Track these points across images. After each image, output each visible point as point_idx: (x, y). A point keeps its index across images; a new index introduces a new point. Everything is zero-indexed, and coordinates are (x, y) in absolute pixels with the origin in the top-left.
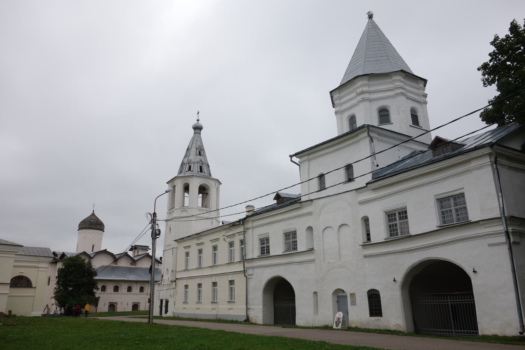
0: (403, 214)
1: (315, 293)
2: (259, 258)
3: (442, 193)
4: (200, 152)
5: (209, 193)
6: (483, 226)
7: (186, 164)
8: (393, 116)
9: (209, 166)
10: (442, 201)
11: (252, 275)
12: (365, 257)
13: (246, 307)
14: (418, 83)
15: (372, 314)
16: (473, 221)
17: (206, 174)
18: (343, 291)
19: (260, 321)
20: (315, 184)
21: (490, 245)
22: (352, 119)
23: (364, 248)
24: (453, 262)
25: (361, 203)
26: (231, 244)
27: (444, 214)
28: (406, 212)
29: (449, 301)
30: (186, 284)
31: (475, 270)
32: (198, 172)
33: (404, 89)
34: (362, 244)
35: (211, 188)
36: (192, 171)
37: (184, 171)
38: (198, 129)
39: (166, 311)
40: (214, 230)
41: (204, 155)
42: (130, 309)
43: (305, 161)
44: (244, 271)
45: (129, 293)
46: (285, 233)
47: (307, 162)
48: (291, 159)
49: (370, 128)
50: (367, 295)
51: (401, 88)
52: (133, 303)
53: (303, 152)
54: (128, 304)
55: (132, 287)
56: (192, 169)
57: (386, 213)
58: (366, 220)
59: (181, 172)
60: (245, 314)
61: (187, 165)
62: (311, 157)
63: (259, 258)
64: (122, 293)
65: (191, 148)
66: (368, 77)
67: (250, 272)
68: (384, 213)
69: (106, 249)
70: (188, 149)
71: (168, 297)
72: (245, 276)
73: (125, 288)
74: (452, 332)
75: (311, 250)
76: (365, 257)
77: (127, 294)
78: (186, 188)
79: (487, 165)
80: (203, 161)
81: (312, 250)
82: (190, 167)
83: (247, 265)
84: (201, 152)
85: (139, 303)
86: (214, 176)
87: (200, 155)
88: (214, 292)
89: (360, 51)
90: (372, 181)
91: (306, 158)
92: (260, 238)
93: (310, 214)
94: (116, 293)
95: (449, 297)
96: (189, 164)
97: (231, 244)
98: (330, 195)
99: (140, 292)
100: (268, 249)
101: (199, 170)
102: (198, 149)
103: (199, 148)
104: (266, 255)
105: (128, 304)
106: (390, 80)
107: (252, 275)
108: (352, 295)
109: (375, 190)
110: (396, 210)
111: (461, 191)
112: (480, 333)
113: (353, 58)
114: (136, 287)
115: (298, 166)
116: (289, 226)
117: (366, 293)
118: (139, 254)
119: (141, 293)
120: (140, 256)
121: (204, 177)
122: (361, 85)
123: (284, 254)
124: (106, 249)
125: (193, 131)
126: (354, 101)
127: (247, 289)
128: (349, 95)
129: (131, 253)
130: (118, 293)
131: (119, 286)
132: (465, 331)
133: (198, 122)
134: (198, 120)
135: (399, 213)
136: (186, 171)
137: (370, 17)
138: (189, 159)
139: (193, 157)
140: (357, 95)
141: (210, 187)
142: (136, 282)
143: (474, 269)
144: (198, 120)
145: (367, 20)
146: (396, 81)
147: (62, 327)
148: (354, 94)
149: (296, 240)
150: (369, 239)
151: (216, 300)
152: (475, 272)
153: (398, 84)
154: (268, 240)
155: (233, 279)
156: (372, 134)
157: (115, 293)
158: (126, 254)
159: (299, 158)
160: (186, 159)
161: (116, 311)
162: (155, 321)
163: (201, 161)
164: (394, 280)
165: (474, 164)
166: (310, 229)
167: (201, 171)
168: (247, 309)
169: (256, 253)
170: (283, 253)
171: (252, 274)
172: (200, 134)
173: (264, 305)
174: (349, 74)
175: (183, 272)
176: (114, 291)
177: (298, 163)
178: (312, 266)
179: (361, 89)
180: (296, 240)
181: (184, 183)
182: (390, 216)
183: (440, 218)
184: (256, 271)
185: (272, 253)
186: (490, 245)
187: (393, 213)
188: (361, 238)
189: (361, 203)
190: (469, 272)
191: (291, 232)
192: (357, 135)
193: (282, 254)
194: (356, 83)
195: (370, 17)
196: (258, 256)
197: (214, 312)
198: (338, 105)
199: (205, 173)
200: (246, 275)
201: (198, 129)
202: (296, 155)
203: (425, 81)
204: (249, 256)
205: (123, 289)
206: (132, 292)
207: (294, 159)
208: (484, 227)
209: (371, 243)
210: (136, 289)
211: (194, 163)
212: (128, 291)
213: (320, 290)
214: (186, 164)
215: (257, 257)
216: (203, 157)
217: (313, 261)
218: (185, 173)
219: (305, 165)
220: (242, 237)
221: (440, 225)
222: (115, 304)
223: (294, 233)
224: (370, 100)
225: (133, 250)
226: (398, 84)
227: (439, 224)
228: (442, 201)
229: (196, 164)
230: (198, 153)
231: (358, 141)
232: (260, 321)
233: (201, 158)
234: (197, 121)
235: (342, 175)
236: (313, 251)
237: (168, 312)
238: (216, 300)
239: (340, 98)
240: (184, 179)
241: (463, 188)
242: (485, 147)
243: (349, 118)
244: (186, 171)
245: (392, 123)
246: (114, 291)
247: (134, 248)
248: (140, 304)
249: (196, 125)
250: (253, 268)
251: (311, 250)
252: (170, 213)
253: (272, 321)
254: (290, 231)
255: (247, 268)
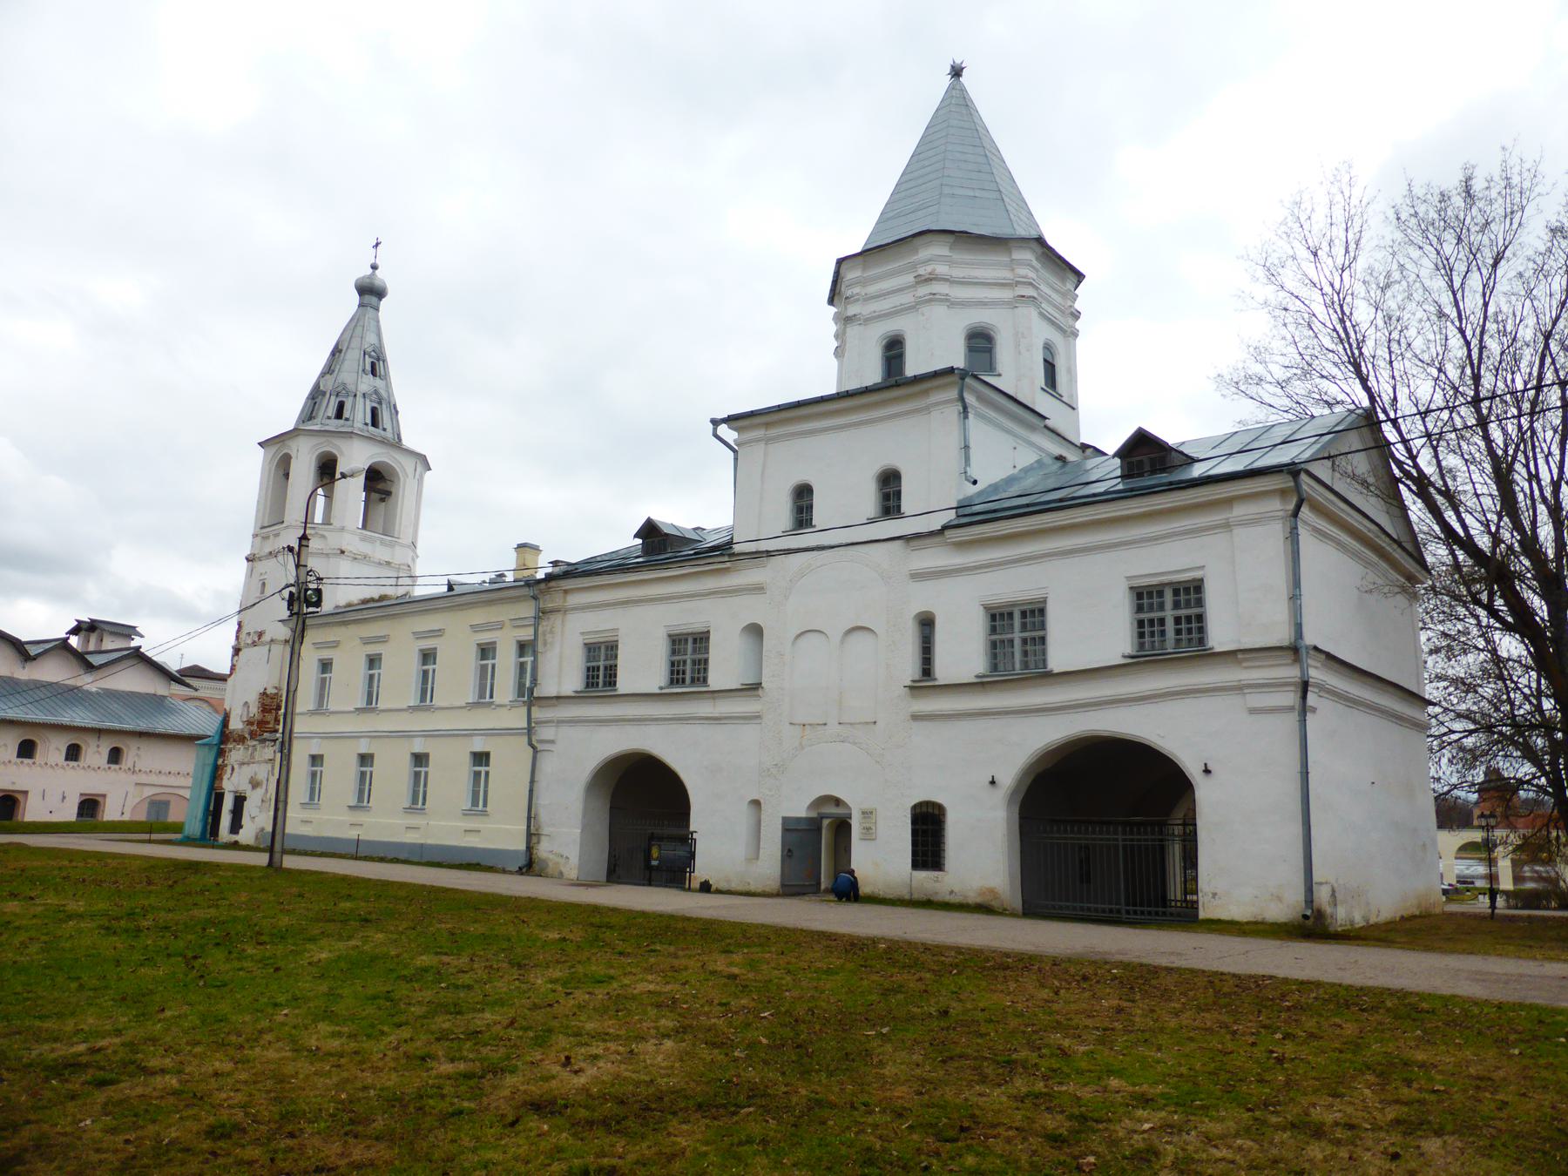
0: (1035, 614)
1: (756, 804)
2: (577, 698)
3: (1147, 572)
4: (373, 365)
5: (393, 490)
6: (1245, 664)
7: (328, 395)
8: (1004, 354)
9: (397, 412)
10: (1145, 596)
11: (552, 742)
12: (916, 717)
13: (525, 827)
14: (1063, 280)
15: (917, 864)
16: (1218, 649)
17: (389, 435)
18: (838, 802)
19: (571, 871)
20: (781, 513)
21: (1253, 711)
22: (894, 350)
23: (913, 696)
24: (1152, 745)
25: (917, 576)
26: (486, 651)
27: (1146, 629)
28: (1042, 612)
29: (1120, 837)
30: (314, 752)
31: (1209, 768)
32: (366, 424)
33: (1037, 288)
34: (909, 683)
35: (402, 479)
36: (347, 419)
37: (321, 413)
38: (370, 292)
39: (236, 826)
40: (427, 603)
41: (385, 378)
42: (69, 813)
43: (758, 440)
44: (530, 731)
45: (72, 764)
46: (670, 636)
47: (762, 445)
48: (715, 430)
49: (968, 380)
50: (909, 816)
51: (1031, 284)
52: (81, 795)
53: (752, 414)
54: (64, 798)
55: (125, 750)
56: (346, 414)
57: (987, 608)
58: (926, 624)
59: (309, 413)
60: (522, 847)
61: (333, 398)
62: (773, 432)
63: (577, 698)
64: (46, 764)
65: (348, 348)
66: (951, 238)
67: (545, 733)
68: (982, 608)
69: (140, 647)
70: (337, 351)
71: (244, 787)
72: (531, 745)
73: (58, 749)
74: (1119, 911)
75: (754, 688)
76: (916, 717)
77: (63, 767)
78: (327, 470)
79: (1274, 518)
80: (384, 394)
81: (756, 689)
82: (341, 406)
83: (537, 713)
84: (376, 365)
85: (104, 796)
86: (408, 441)
87: (374, 372)
88: (418, 782)
89: (926, 163)
90: (956, 522)
91: (759, 433)
92: (586, 641)
93: (758, 589)
94: (26, 761)
95: (1120, 829)
96: (337, 395)
97: (486, 651)
98: (833, 543)
99: (110, 762)
100: (610, 675)
101: (369, 420)
102: (370, 356)
103: (373, 353)
104: (601, 690)
105: (64, 798)
106: (1004, 258)
107: (552, 742)
108: (867, 814)
109: (961, 545)
110: (1014, 604)
111: (1197, 574)
112: (1202, 915)
113: (904, 179)
114: (98, 746)
115: (732, 453)
116: (688, 617)
117: (909, 811)
118: (104, 648)
119: (113, 766)
120: (107, 655)
121: (384, 442)
122: (934, 256)
123: (664, 691)
124: (140, 647)
125: (356, 298)
126: (906, 298)
127: (532, 782)
128: (892, 279)
129: (74, 641)
130: (34, 763)
131: (38, 741)
132: (1146, 909)
133: (373, 274)
134: (374, 267)
135: (1024, 614)
136: (329, 418)
137: (957, 72)
138: (340, 380)
139: (350, 373)
140: (917, 283)
141: (401, 475)
142: (99, 732)
143: (1206, 764)
144: (374, 267)
145: (946, 81)
146: (1021, 263)
147: (760, 1042)
148: (909, 278)
149: (705, 656)
150: (927, 669)
151: (420, 803)
152: (1207, 771)
153: (1023, 271)
154: (612, 648)
155: (486, 750)
156: (970, 399)
157: (22, 762)
158: (63, 645)
159: (735, 429)
160: (330, 379)
161: (20, 818)
162: (290, 862)
163: (376, 392)
164: (993, 782)
165: (1239, 511)
166: (755, 631)
167: (375, 423)
168: (530, 835)
169: (573, 681)
170: (661, 688)
171: (551, 738)
172: (377, 310)
173: (584, 828)
174: (888, 219)
175: (405, 715)
176: (19, 756)
177: (733, 444)
178: (748, 732)
179: (929, 269)
180: (705, 656)
181: (317, 453)
182: (998, 617)
183: (1132, 637)
184: (566, 732)
185: (624, 684)
186: (1253, 711)
187: (1009, 610)
188: (909, 668)
189: (917, 576)
190: (1192, 768)
191: (692, 634)
192: (926, 392)
193: (658, 691)
194: (916, 251)
195: (957, 72)
196: (576, 692)
197: (352, 834)
198: (858, 300)
199: (384, 430)
200: (534, 743)
201: (370, 292)
202: (731, 420)
203: (1079, 276)
204: (547, 688)
205: (52, 750)
206: (82, 763)
207: (723, 430)
208: (1246, 668)
209: (937, 683)
210: (96, 753)
211: (355, 396)
212: (67, 759)
213: (772, 796)
214: (328, 395)
215: (573, 695)
216: (384, 382)
217: (756, 717)
218: (324, 421)
219: (755, 454)
220: (526, 634)
221: (1135, 653)
222: (20, 797)
223: (701, 640)
224: (952, 303)
225: (83, 634)
226: (1023, 271)
227: (1129, 650)
228: (1145, 596)
229: (362, 400)
230: (368, 367)
231: (927, 409)
232: (571, 871)
233: (378, 382)
234: (371, 270)
235: (868, 499)
236: (760, 692)
237: (241, 831)
238: (420, 803)
239: (863, 282)
240: (322, 440)
241: (1204, 566)
242: (1281, 471)
243: (884, 342)
244: (329, 418)
245: (1000, 375)
246: (19, 756)
247: (86, 628)
248: (108, 800)
249: (368, 280)
250: (560, 722)
251: (754, 688)
252: (265, 538)
253: (602, 872)
254: (690, 631)
255: (536, 723)
